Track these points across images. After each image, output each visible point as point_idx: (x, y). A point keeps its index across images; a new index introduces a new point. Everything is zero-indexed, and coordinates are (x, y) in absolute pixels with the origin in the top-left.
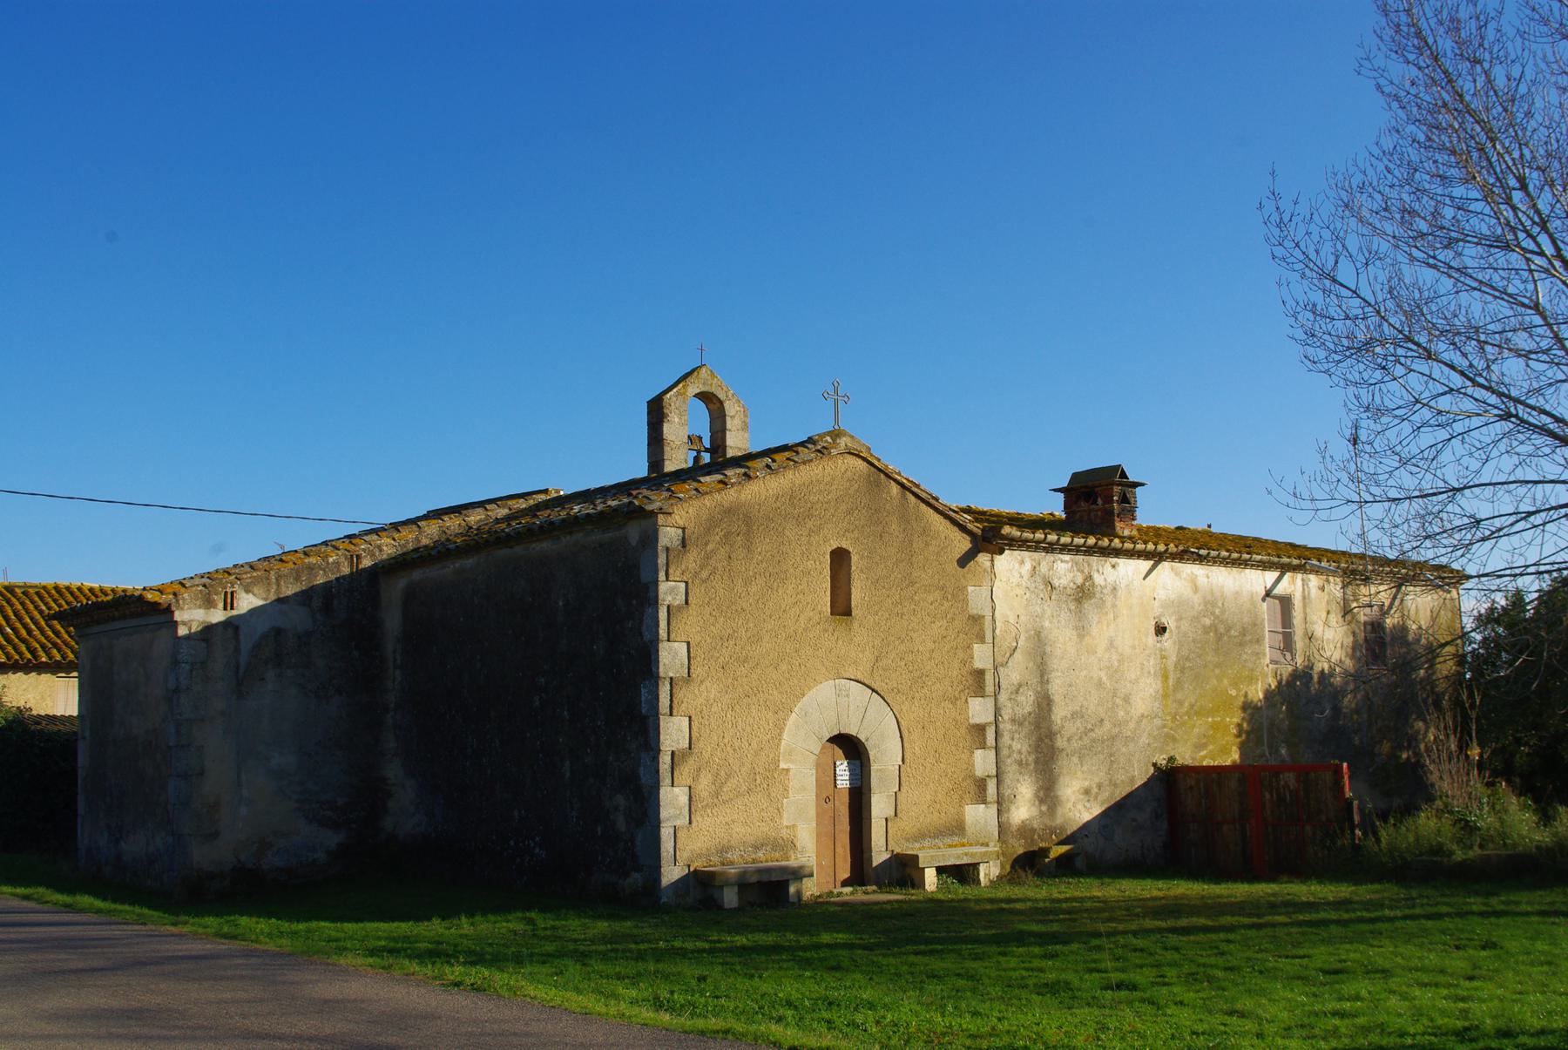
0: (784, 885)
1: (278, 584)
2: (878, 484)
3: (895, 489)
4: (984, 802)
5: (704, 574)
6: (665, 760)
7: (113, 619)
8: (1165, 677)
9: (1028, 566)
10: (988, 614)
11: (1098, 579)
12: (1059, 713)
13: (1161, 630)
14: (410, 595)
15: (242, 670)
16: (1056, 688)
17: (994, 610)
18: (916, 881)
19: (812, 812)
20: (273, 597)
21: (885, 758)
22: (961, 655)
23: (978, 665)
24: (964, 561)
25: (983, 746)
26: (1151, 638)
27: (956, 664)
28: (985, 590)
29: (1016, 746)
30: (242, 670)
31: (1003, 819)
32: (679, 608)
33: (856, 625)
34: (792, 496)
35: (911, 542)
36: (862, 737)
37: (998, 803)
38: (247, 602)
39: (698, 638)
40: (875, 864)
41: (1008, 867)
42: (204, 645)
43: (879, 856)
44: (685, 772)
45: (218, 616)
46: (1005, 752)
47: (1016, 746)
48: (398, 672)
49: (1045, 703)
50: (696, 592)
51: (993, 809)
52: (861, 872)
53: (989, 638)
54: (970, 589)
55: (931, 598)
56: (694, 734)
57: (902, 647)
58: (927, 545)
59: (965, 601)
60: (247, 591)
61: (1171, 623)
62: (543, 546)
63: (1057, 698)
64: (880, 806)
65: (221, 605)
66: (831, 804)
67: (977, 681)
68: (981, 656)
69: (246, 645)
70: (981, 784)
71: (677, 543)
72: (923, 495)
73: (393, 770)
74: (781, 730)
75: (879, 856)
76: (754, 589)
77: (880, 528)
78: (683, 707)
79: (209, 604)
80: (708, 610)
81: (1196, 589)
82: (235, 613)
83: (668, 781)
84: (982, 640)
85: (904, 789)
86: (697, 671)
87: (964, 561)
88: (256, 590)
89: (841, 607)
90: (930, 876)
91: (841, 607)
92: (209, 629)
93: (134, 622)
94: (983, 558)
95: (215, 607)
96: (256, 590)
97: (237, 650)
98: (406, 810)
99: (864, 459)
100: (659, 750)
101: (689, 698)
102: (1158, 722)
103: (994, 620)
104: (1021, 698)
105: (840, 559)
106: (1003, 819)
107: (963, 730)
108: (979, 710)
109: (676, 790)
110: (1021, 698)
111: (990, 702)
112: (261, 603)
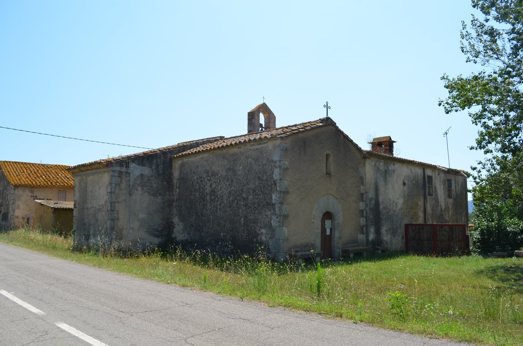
7: (88, 170)
8: (405, 198)
9: (373, 163)
11: (390, 169)
12: (381, 207)
13: (404, 184)
14: (182, 166)
16: (381, 198)
19: (320, 236)
25: (363, 217)
26: (402, 186)
29: (371, 217)
33: (332, 178)
36: (333, 213)
46: (368, 218)
47: (371, 217)
48: (177, 190)
49: (377, 203)
51: (365, 235)
61: (406, 182)
62: (235, 150)
63: (380, 203)
65: (125, 166)
70: (362, 228)
73: (176, 220)
81: (412, 173)
93: (95, 171)
96: (135, 161)
98: (179, 232)
102: (403, 211)
104: (372, 202)
105: (327, 156)
110: (372, 202)
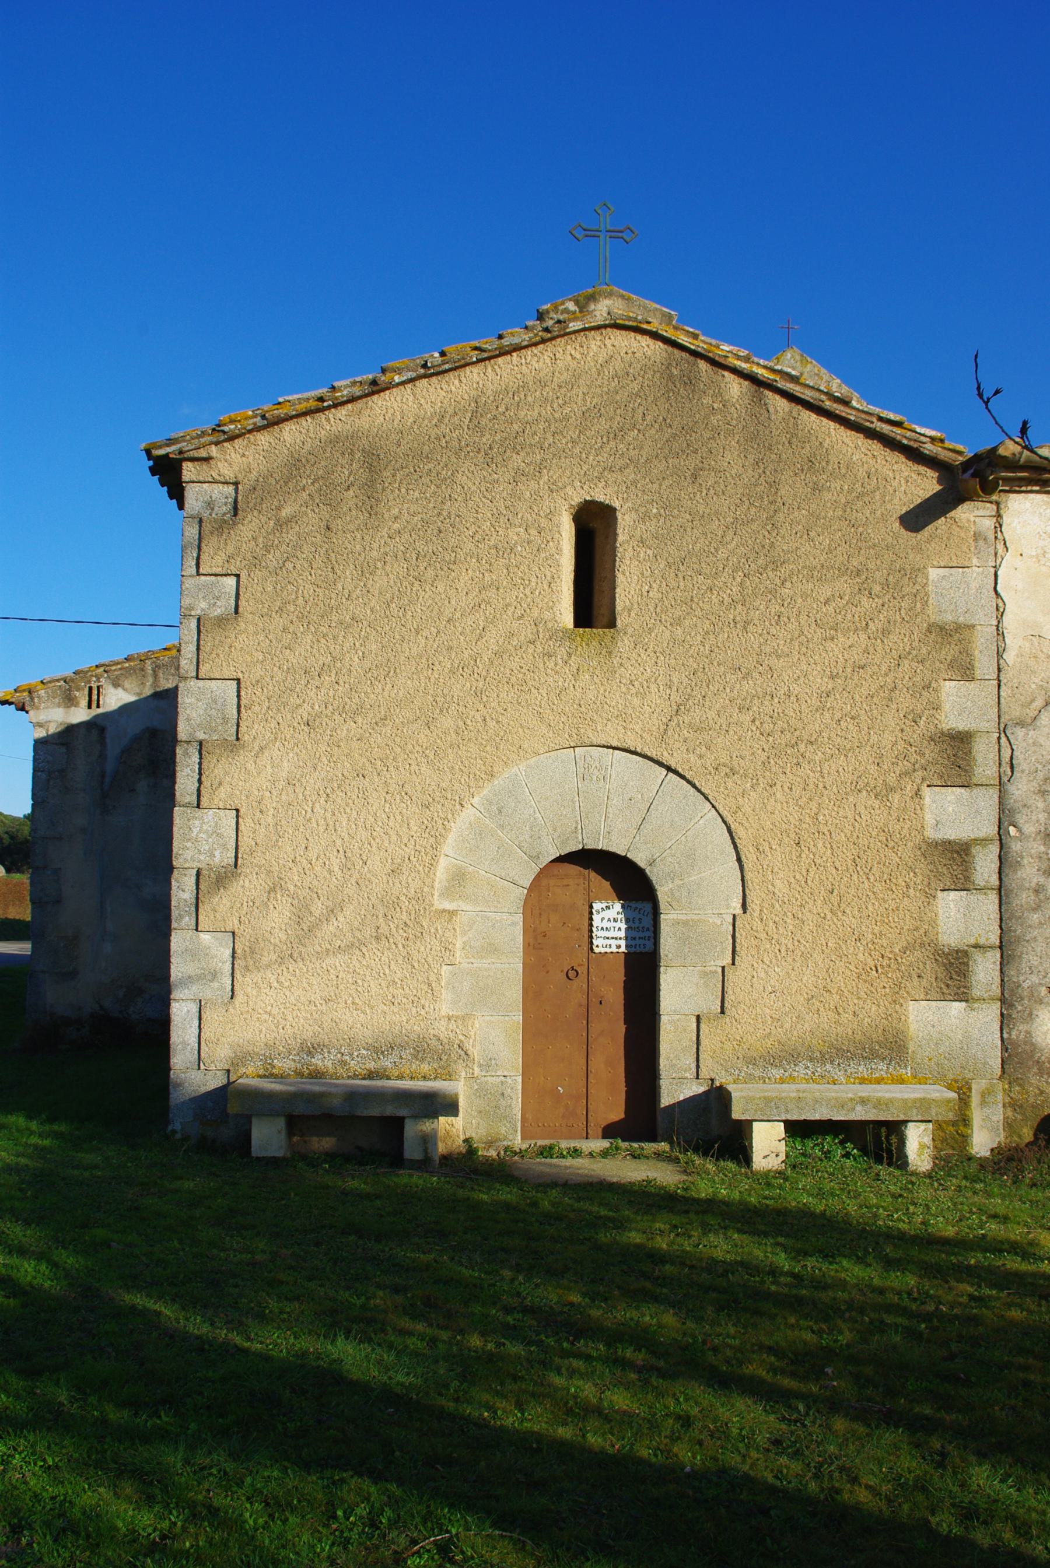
0: (396, 1125)
1: (155, 675)
2: (690, 381)
3: (735, 388)
4: (963, 996)
5: (272, 560)
6: (182, 890)
10: (985, 623)
15: (107, 780)
17: (1000, 613)
18: (735, 1142)
20: (148, 691)
21: (697, 899)
22: (905, 701)
23: (952, 720)
24: (917, 519)
27: (891, 720)
28: (977, 576)
30: (107, 780)
31: (1017, 1033)
32: (221, 622)
33: (624, 644)
34: (478, 410)
35: (774, 485)
36: (640, 858)
37: (1003, 1000)
38: (115, 698)
39: (258, 672)
40: (666, 1101)
41: (1027, 1134)
42: (63, 750)
43: (677, 1085)
44: (221, 906)
45: (80, 715)
50: (255, 585)
52: (642, 1117)
53: (984, 666)
54: (934, 574)
55: (826, 591)
56: (246, 841)
57: (747, 686)
58: (816, 488)
59: (921, 596)
60: (116, 685)
64: (678, 993)
65: (84, 702)
66: (580, 983)
67: (953, 756)
68: (959, 705)
69: (113, 750)
71: (223, 509)
72: (808, 395)
74: (438, 840)
75: (677, 1085)
76: (379, 582)
77: (693, 462)
78: (223, 793)
79: (69, 701)
80: (279, 622)
82: (100, 711)
83: (188, 921)
84: (965, 672)
85: (742, 961)
86: (254, 730)
87: (917, 519)
88: (127, 684)
89: (592, 605)
90: (768, 1144)
91: (592, 605)
92: (70, 731)
94: (972, 515)
95: (77, 705)
96: (127, 684)
97: (102, 756)
99: (655, 336)
100: (171, 869)
101: (234, 779)
103: (1000, 633)
105: (594, 529)
106: (1017, 1033)
107: (907, 852)
108: (954, 813)
109: (205, 937)
111: (987, 801)
112: (133, 698)
